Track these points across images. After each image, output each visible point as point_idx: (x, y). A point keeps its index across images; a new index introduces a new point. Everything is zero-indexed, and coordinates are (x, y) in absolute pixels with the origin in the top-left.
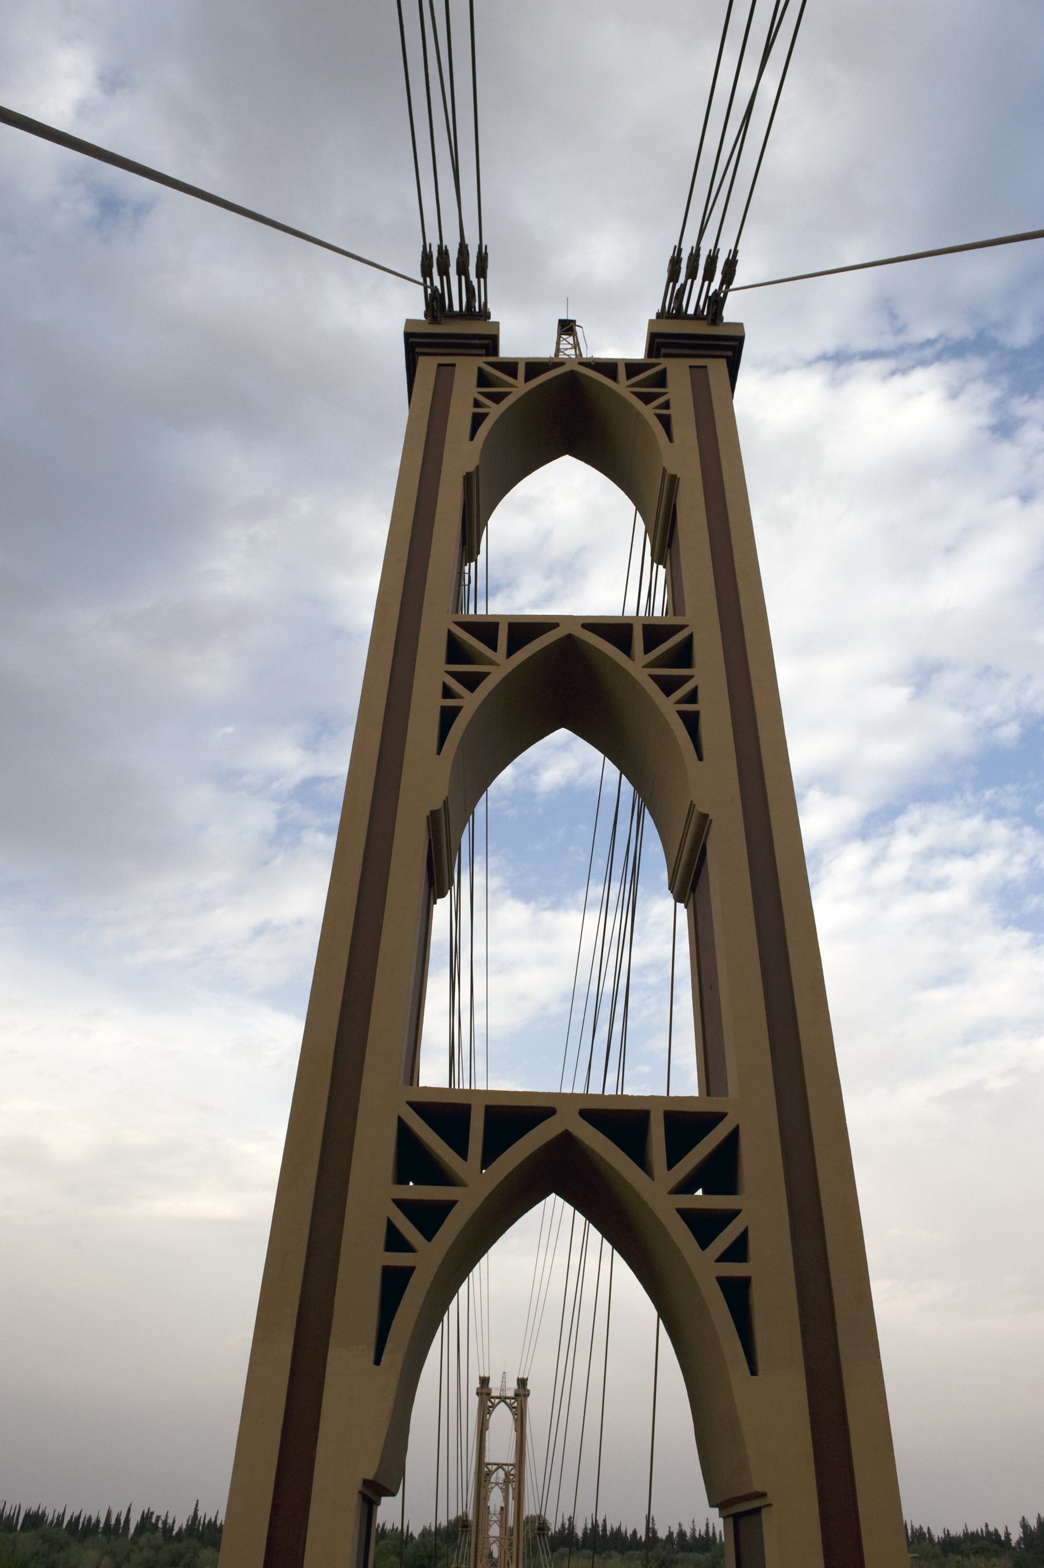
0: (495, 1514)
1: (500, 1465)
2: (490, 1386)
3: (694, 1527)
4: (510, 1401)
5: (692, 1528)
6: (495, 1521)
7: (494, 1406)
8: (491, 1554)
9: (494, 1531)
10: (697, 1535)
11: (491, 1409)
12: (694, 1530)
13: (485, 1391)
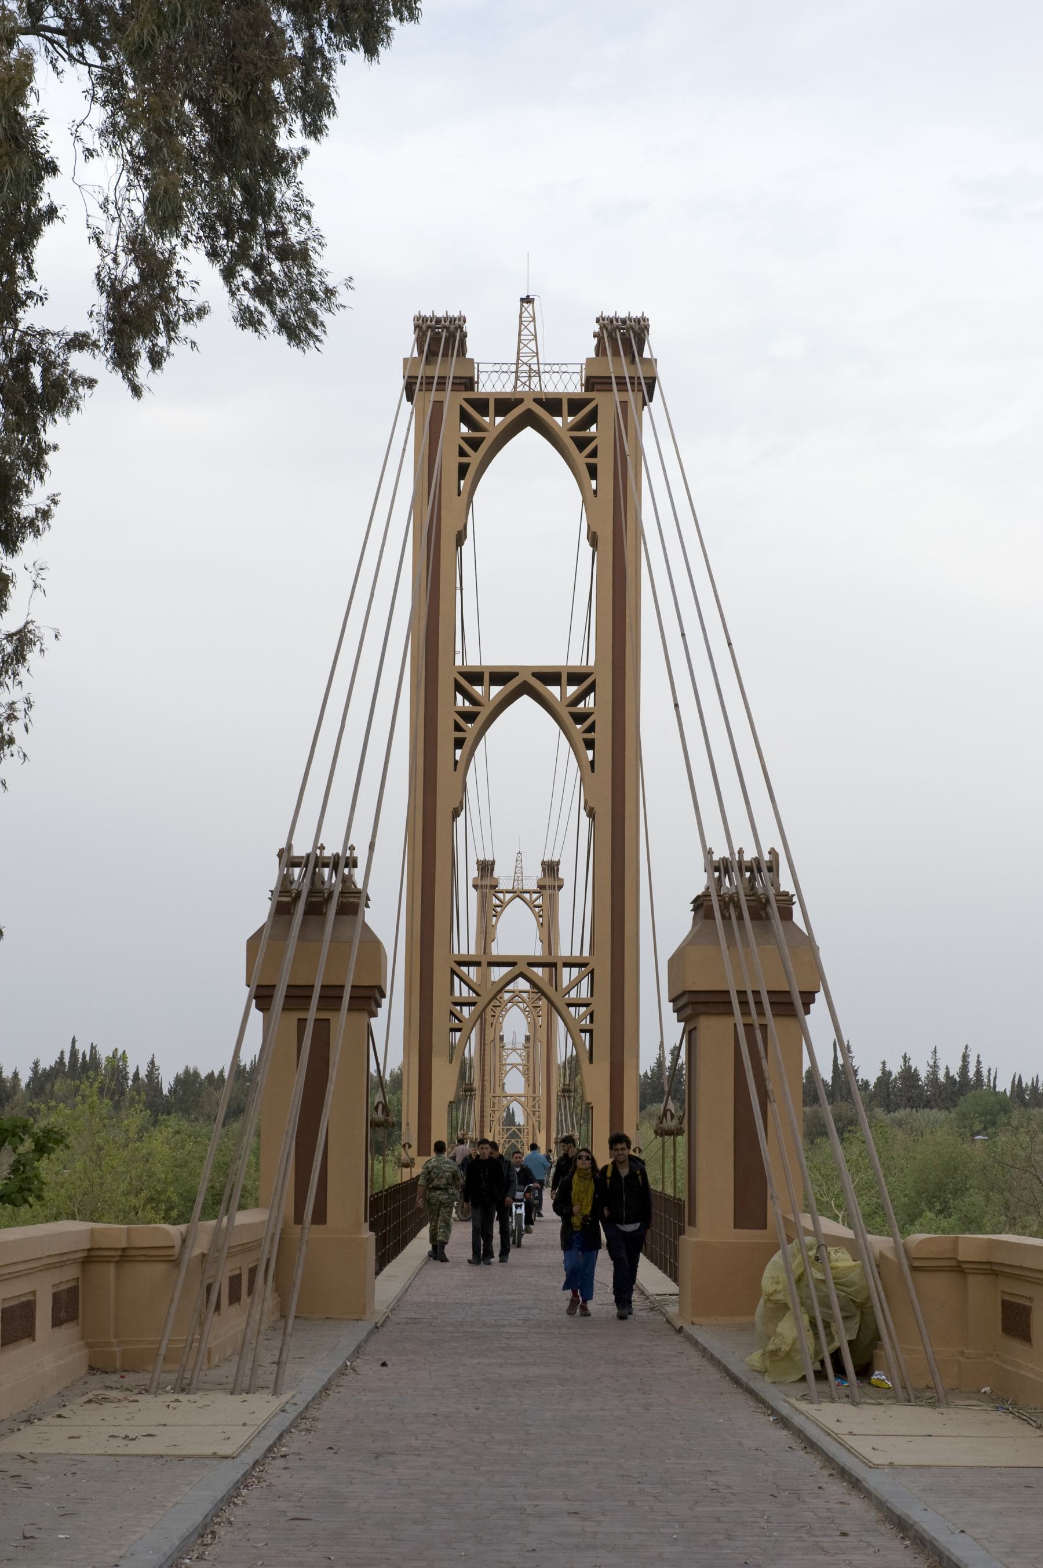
0: (514, 1050)
1: (522, 967)
2: (496, 874)
3: (935, 1063)
4: (563, 693)
5: (931, 1063)
6: (514, 1065)
7: (503, 905)
8: (510, 1118)
9: (515, 1083)
10: (941, 1076)
11: (499, 909)
12: (935, 1067)
13: (488, 882)
